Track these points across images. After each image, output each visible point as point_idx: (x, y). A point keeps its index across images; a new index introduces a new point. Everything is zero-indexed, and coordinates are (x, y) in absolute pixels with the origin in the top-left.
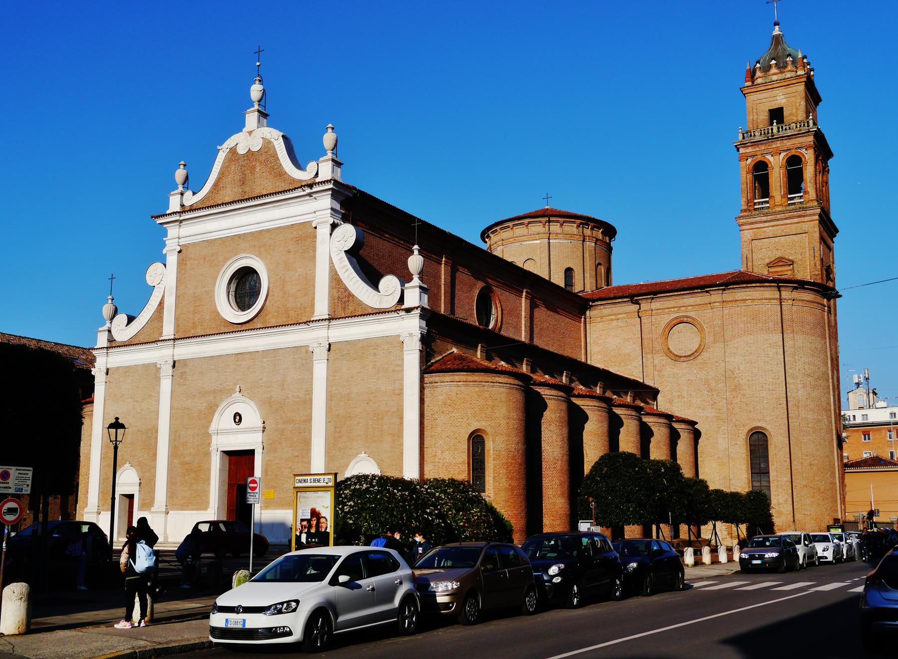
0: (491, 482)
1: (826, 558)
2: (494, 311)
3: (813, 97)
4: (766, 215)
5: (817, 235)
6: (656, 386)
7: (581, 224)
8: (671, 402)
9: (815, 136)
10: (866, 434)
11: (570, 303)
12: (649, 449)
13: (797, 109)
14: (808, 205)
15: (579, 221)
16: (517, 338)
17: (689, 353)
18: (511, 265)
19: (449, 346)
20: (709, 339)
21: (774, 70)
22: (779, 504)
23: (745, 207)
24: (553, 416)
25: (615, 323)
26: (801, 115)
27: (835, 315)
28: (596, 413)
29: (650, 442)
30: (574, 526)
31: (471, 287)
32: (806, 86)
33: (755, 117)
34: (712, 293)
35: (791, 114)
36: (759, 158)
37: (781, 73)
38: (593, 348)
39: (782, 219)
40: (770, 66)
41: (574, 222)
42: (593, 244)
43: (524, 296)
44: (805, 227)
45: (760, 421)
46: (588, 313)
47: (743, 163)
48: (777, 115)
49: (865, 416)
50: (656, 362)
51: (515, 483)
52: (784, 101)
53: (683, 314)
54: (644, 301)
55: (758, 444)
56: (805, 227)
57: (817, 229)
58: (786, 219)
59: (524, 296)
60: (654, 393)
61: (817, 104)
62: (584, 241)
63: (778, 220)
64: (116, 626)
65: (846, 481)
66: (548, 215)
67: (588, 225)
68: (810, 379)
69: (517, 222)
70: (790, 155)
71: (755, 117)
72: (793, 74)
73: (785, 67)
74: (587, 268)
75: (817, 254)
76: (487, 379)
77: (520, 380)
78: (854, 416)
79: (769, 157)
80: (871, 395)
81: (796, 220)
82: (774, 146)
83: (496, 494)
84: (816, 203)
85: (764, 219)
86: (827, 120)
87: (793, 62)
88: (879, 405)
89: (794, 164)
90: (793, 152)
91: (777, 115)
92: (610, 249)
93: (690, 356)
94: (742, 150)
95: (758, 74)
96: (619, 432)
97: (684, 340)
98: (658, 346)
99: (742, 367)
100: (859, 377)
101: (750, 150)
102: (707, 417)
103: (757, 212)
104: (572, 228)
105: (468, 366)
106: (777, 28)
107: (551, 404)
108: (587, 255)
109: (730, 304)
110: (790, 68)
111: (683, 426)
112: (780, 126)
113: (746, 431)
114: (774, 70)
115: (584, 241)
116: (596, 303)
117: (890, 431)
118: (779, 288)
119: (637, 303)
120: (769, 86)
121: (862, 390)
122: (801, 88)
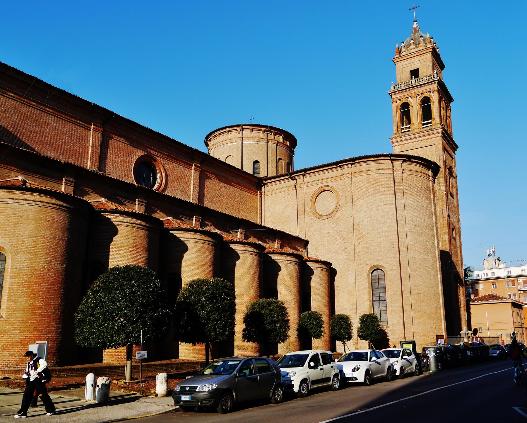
0: (5, 301)
1: (356, 379)
2: (159, 176)
4: (408, 135)
5: (441, 146)
6: (307, 238)
7: (265, 131)
8: (316, 249)
10: (494, 284)
11: (254, 183)
12: (277, 281)
14: (435, 127)
15: (264, 129)
17: (329, 213)
18: (218, 161)
19: (12, 174)
20: (342, 201)
21: (413, 46)
22: (393, 324)
23: (396, 132)
24: (125, 242)
25: (280, 194)
26: (430, 72)
27: (457, 200)
28: (198, 245)
29: (235, 265)
31: (129, 154)
33: (402, 76)
34: (344, 167)
35: (424, 72)
36: (404, 100)
37: (417, 47)
38: (266, 214)
39: (419, 137)
40: (410, 44)
42: (275, 145)
43: (193, 169)
44: (433, 141)
45: (378, 260)
46: (263, 188)
47: (394, 105)
48: (415, 73)
50: (307, 221)
51: (38, 303)
53: (325, 184)
54: (299, 177)
55: (376, 277)
56: (433, 141)
58: (421, 137)
59: (193, 169)
60: (305, 243)
61: (442, 69)
62: (268, 143)
63: (416, 138)
64: (215, 386)
65: (471, 311)
66: (242, 127)
67: (271, 132)
68: (417, 228)
69: (222, 131)
70: (423, 96)
71: (402, 76)
72: (424, 48)
73: (419, 44)
74: (270, 161)
76: (12, 196)
77: (209, 237)
78: (487, 274)
79: (410, 99)
80: (497, 261)
81: (427, 137)
82: (413, 92)
83: (9, 314)
84: (440, 126)
85: (407, 138)
86: (447, 77)
87: (424, 41)
89: (426, 102)
90: (425, 95)
91: (415, 73)
92: (293, 152)
93: (329, 215)
94: (393, 96)
95: (403, 50)
96: (236, 264)
97: (326, 204)
98: (308, 209)
100: (490, 251)
101: (398, 95)
102: (341, 259)
103: (403, 134)
104: (259, 134)
105: (105, 209)
106: (415, 23)
107: (123, 230)
108: (270, 152)
109: (356, 174)
110: (422, 44)
111: (316, 265)
112: (416, 79)
113: (368, 269)
114: (413, 46)
115: (268, 143)
116: (268, 181)
118: (392, 160)
120: (410, 56)
121: (491, 259)
122: (429, 56)
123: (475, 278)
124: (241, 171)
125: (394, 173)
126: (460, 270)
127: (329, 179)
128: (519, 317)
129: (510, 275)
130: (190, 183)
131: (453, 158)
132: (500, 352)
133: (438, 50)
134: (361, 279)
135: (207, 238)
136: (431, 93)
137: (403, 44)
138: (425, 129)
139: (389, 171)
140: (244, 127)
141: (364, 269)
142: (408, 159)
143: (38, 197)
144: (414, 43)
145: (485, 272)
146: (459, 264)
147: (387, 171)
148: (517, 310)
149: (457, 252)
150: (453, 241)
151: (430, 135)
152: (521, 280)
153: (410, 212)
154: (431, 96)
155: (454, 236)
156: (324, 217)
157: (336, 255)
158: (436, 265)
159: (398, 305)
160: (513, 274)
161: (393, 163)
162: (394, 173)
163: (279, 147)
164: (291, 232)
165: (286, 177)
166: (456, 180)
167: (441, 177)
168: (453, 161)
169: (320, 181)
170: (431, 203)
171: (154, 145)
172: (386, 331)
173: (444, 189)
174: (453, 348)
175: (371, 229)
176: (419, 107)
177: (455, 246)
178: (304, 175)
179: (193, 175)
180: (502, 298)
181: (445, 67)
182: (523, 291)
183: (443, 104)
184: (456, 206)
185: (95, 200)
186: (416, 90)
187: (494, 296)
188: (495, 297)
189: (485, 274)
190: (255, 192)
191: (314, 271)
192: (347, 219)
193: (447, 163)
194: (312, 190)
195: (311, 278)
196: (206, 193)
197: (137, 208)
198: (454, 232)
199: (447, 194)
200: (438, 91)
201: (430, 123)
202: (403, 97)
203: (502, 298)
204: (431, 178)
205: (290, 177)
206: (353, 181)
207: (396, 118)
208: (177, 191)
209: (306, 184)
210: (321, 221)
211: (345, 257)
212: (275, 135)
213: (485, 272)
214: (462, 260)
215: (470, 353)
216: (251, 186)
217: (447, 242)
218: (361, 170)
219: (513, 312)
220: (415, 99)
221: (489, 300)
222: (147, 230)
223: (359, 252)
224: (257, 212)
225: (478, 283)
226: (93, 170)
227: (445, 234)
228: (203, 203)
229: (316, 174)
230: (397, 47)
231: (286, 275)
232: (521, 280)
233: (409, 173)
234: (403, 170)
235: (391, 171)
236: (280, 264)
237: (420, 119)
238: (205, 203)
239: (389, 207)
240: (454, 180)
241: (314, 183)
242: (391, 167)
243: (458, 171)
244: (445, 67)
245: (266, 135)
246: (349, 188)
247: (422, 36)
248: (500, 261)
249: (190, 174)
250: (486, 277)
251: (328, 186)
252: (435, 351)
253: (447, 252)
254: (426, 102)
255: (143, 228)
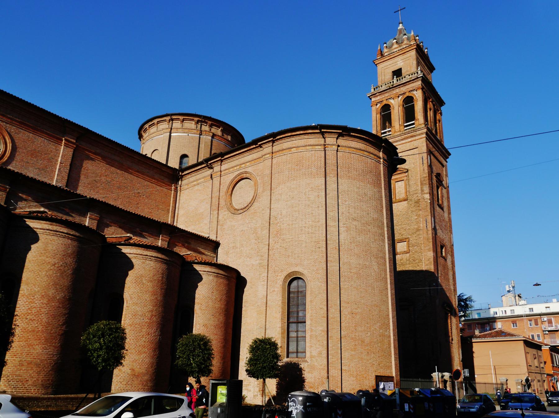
3: (423, 57)
5: (424, 149)
8: (227, 253)
9: (422, 81)
10: (514, 323)
12: (124, 283)
13: (411, 67)
15: (196, 119)
16: (49, 182)
18: (145, 156)
20: (260, 190)
21: (395, 46)
22: (312, 357)
25: (196, 188)
26: (414, 69)
27: (449, 213)
29: (127, 275)
30: (378, 385)
32: (417, 51)
33: (383, 78)
34: (264, 146)
35: (407, 71)
37: (400, 46)
38: (180, 212)
40: (393, 44)
41: (193, 120)
42: (210, 138)
49: (512, 311)
52: (402, 63)
53: (243, 170)
56: (415, 144)
57: (425, 144)
58: (402, 140)
60: (215, 246)
61: (432, 72)
67: (206, 123)
68: (355, 223)
70: (405, 96)
71: (383, 78)
73: (402, 43)
75: (425, 162)
77: (163, 254)
78: (505, 311)
80: (517, 297)
81: (409, 140)
86: (435, 79)
88: (521, 303)
89: (409, 101)
90: (407, 94)
91: (398, 73)
94: (373, 99)
95: (385, 50)
96: (29, 249)
99: (284, 212)
100: (509, 287)
101: (378, 98)
102: (253, 265)
104: (191, 125)
108: (202, 146)
110: (405, 42)
111: (208, 269)
112: (398, 79)
113: (283, 277)
115: (200, 135)
117: (530, 320)
118: (323, 134)
119: (212, 168)
120: (392, 56)
121: (511, 295)
122: (413, 53)
123: (492, 316)
124: (166, 166)
125: (325, 151)
126: (453, 297)
127: (248, 164)
128: (536, 361)
129: (531, 313)
130: (57, 161)
131: (443, 166)
132: (481, 406)
133: (426, 50)
134: (274, 291)
135: (221, 272)
136: (415, 92)
137: (385, 45)
138: (407, 131)
139: (320, 147)
140: (174, 117)
141: (278, 277)
142: (345, 132)
143: (153, 253)
144: (397, 42)
145: (503, 309)
146: (450, 289)
147: (317, 147)
148: (534, 351)
149: (447, 274)
150: (441, 260)
151: (412, 136)
152: (545, 319)
153: (346, 201)
154: (414, 95)
155: (444, 254)
156: (239, 212)
157: (248, 259)
158: (386, 275)
159: (321, 328)
160: (535, 312)
161: (324, 138)
162: (325, 151)
163: (215, 141)
164: (203, 232)
165: (203, 166)
166: (448, 193)
167: (425, 184)
168: (444, 169)
169: (238, 167)
170: (380, 192)
171: (88, 144)
172: (302, 366)
173: (429, 198)
174: (312, 395)
175: (291, 223)
176: (401, 108)
177: (445, 267)
178: (222, 161)
179: (62, 153)
180: (512, 335)
181: (434, 69)
182: (549, 331)
183: (430, 105)
184: (447, 219)
185: (113, 233)
186: (397, 91)
187: (503, 332)
188: (503, 334)
189: (504, 312)
190: (168, 185)
191: (203, 277)
192: (263, 212)
193: (434, 168)
194: (228, 179)
195: (197, 287)
196: (82, 177)
197: (160, 243)
198: (444, 250)
199: (432, 204)
200: (422, 89)
201: (413, 124)
202: (383, 99)
203: (512, 335)
204: (382, 160)
205: (207, 166)
206: (274, 162)
207: (375, 122)
208: (30, 169)
209: (223, 173)
210: (236, 216)
211: (257, 262)
212: (211, 126)
213: (503, 309)
214: (455, 284)
215: (409, 407)
216: (162, 177)
217: (432, 260)
218: (284, 148)
219: (526, 353)
220: (396, 100)
221: (496, 336)
222: (165, 263)
223: (274, 254)
224: (169, 210)
225: (495, 322)
226: (59, 185)
227: (429, 251)
228: (76, 188)
229: (235, 158)
230: (379, 48)
231: (142, 276)
232: (545, 319)
233: (347, 150)
234: (338, 146)
235: (322, 147)
236: (134, 261)
237: (401, 121)
238: (80, 188)
239: (316, 194)
240: (444, 191)
241: (231, 170)
242: (323, 143)
243: (450, 180)
244: (434, 69)
245: (199, 126)
246: (268, 172)
247: (405, 34)
248: (520, 297)
249: (58, 151)
250: (504, 315)
251: (246, 173)
252: (304, 403)
253: (431, 272)
254: (409, 101)
255: (163, 261)
